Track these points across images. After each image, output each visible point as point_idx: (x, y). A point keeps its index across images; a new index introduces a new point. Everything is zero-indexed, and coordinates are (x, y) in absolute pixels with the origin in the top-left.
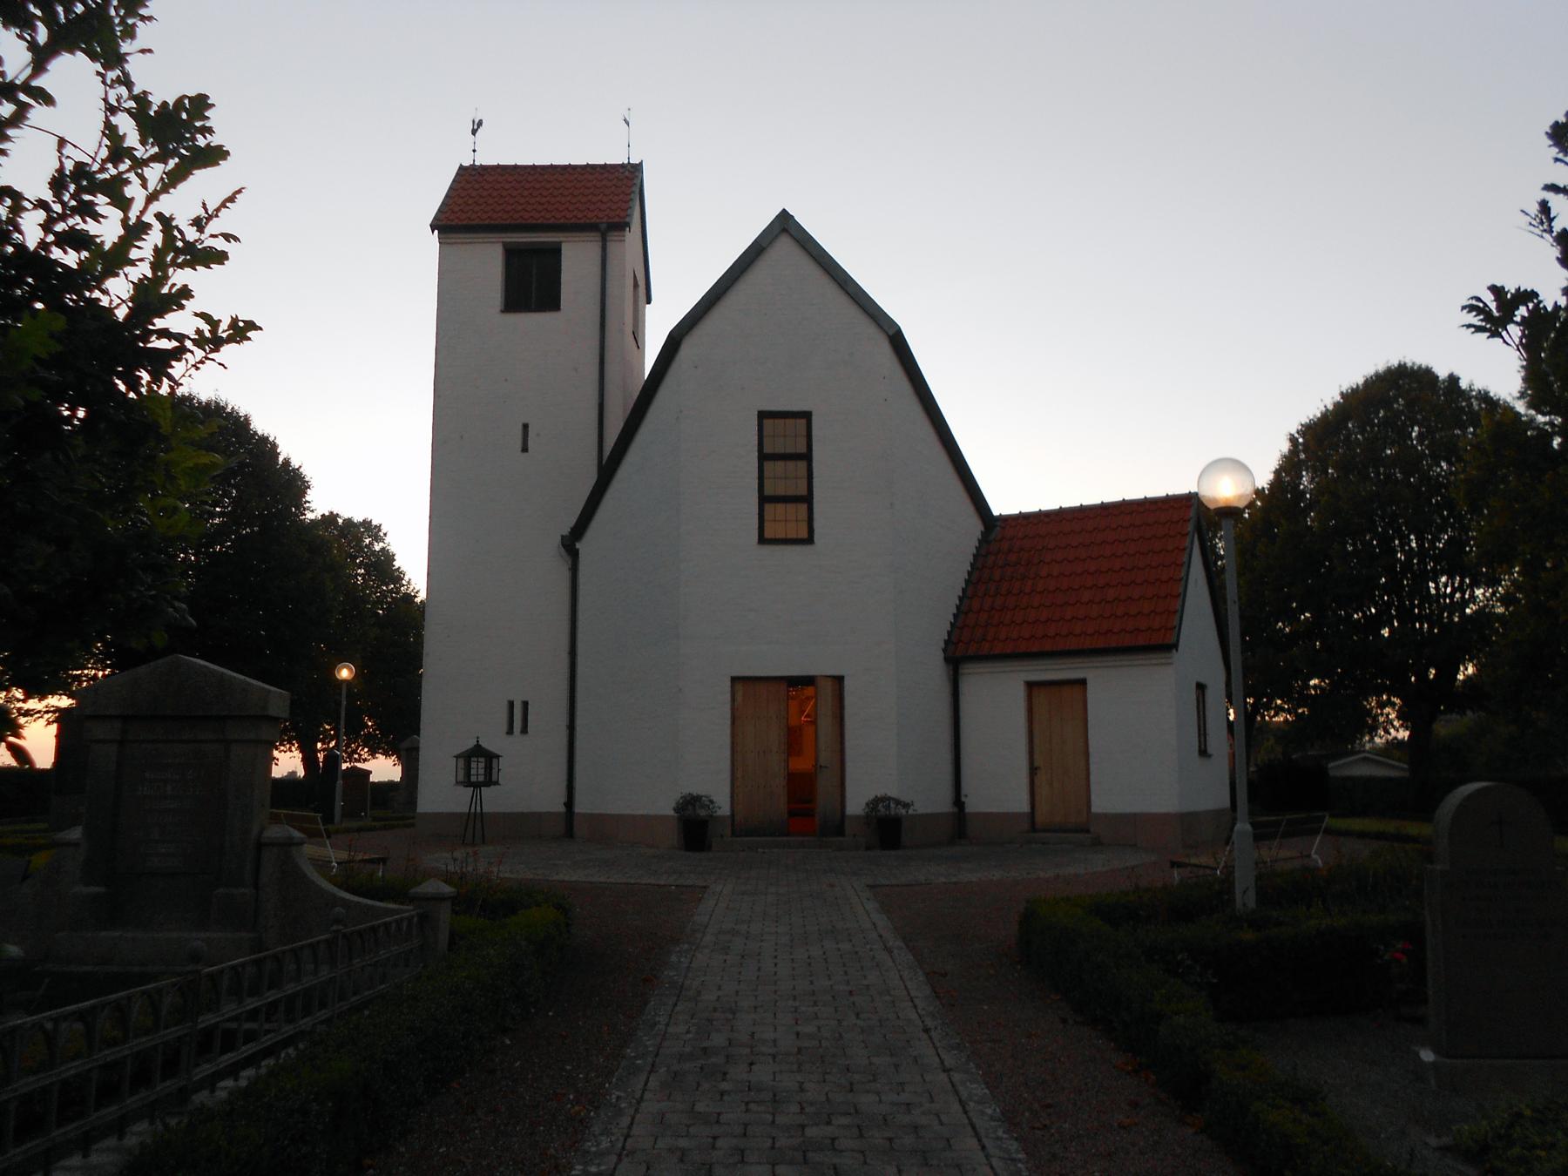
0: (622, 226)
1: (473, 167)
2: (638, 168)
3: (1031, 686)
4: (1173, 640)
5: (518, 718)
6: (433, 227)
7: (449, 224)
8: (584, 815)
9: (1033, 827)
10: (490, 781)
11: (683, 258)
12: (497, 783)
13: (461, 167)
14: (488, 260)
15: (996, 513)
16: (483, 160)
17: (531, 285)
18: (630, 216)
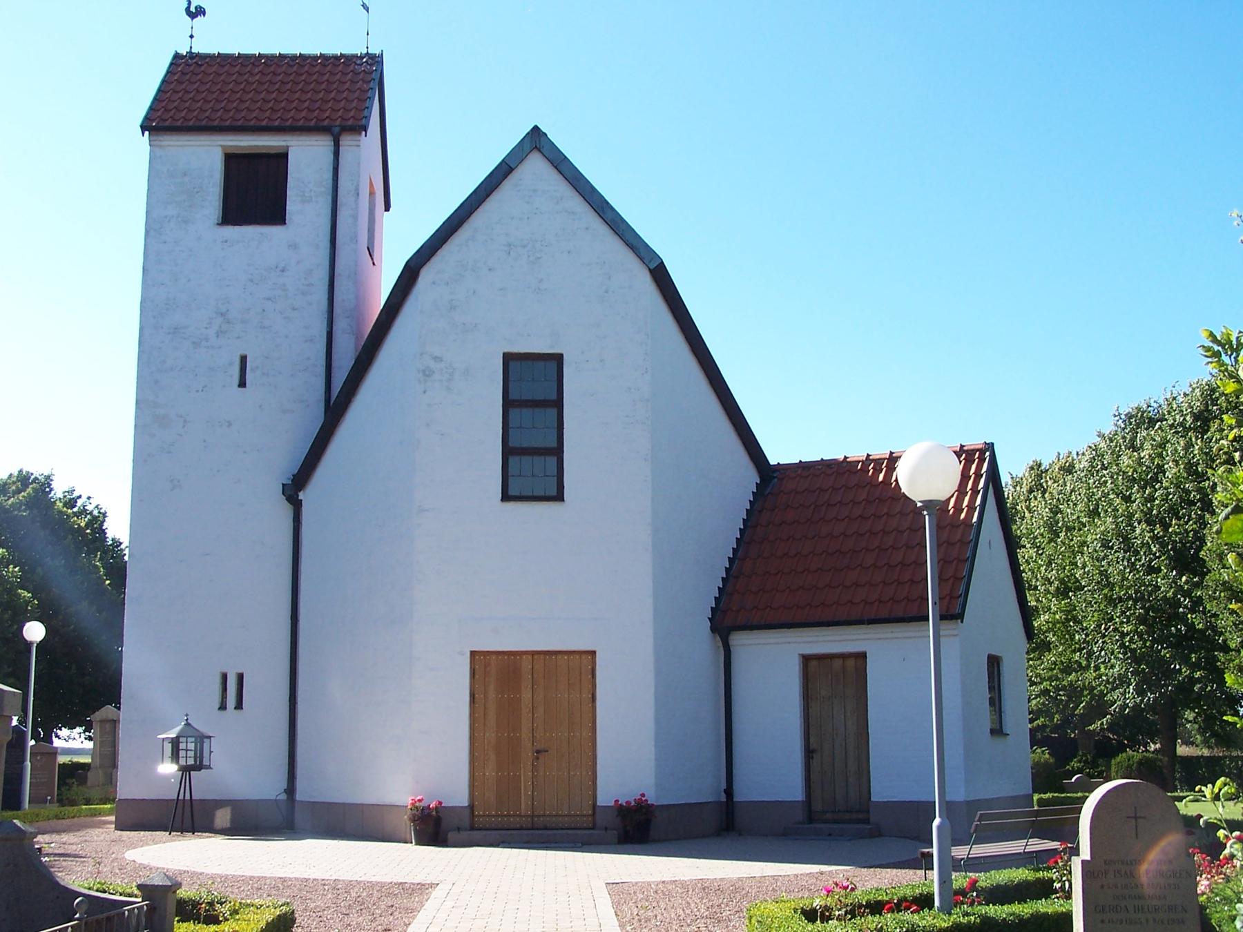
0: (360, 128)
1: (191, 56)
2: (375, 61)
3: (806, 659)
4: (957, 611)
5: (233, 693)
6: (144, 128)
7: (162, 120)
8: (313, 805)
9: (811, 817)
10: (199, 766)
11: (426, 163)
12: (209, 767)
13: (177, 56)
14: (205, 156)
15: (773, 461)
16: (201, 47)
17: (254, 194)
18: (368, 118)
